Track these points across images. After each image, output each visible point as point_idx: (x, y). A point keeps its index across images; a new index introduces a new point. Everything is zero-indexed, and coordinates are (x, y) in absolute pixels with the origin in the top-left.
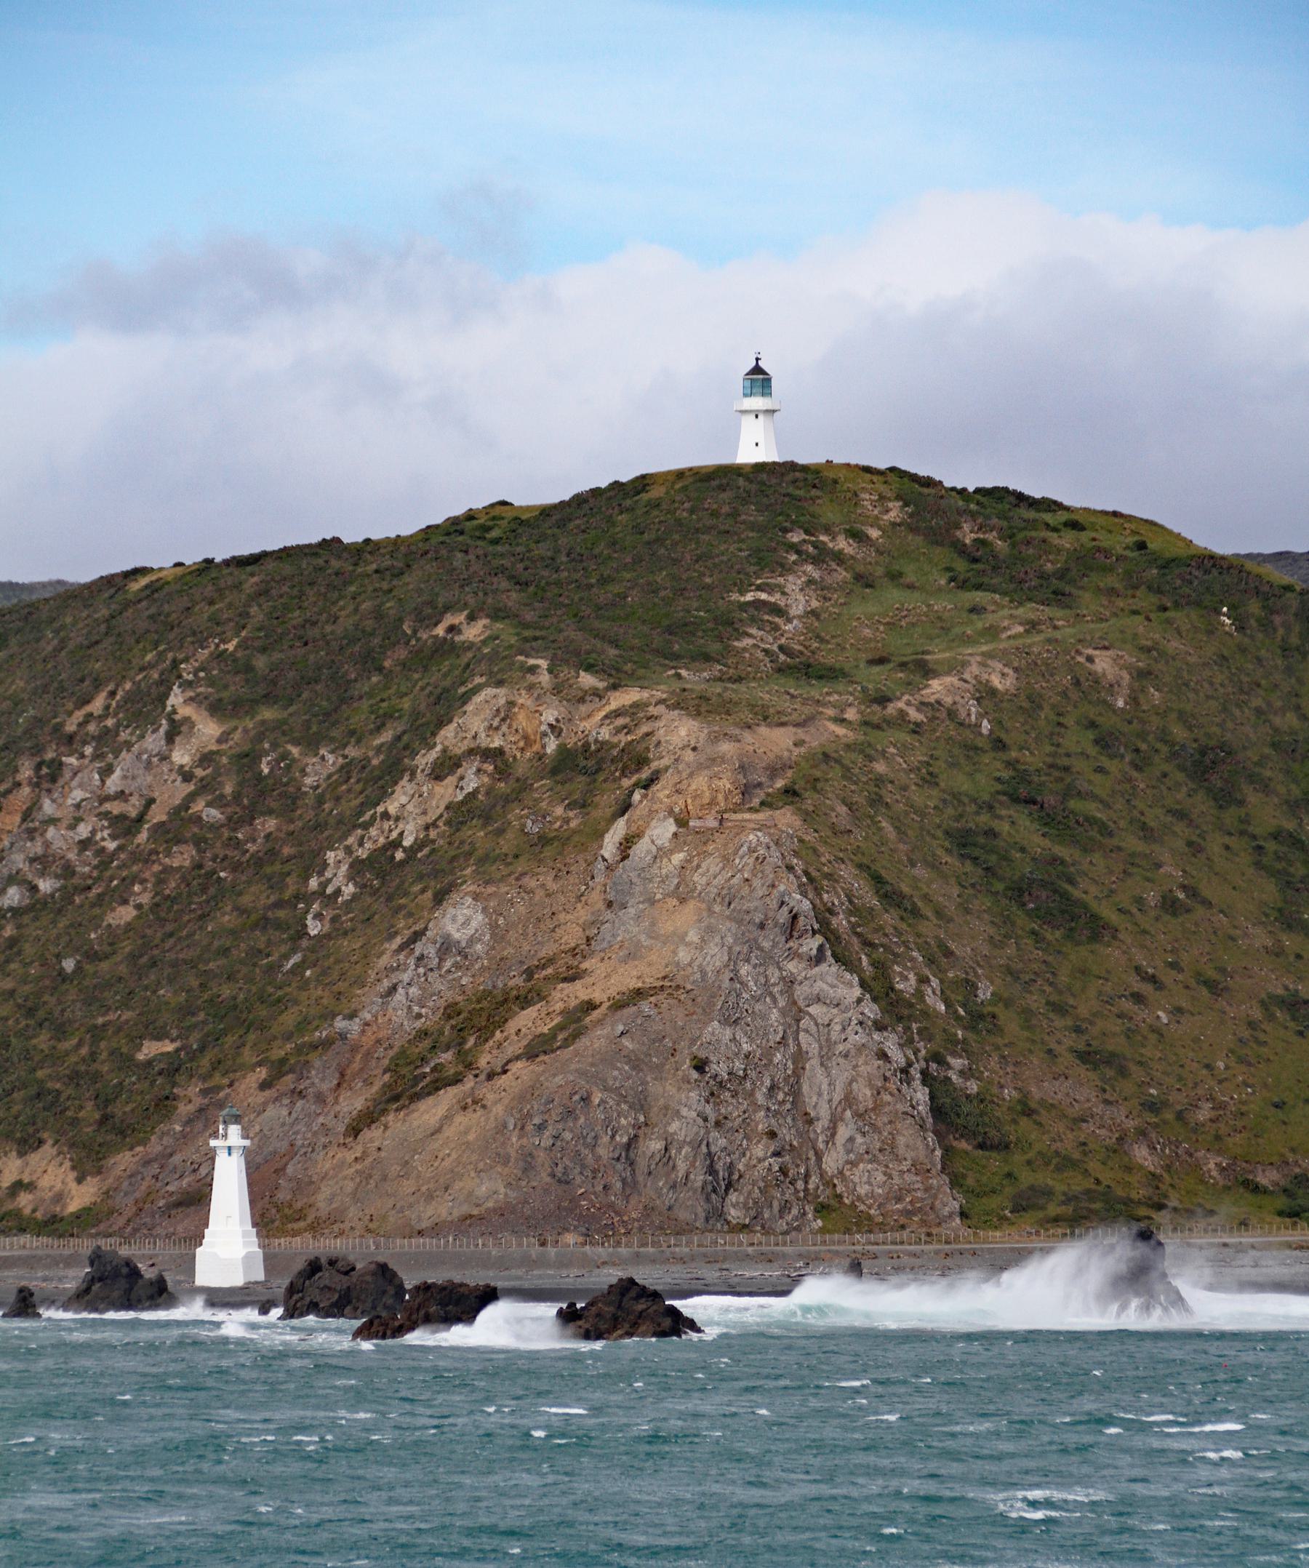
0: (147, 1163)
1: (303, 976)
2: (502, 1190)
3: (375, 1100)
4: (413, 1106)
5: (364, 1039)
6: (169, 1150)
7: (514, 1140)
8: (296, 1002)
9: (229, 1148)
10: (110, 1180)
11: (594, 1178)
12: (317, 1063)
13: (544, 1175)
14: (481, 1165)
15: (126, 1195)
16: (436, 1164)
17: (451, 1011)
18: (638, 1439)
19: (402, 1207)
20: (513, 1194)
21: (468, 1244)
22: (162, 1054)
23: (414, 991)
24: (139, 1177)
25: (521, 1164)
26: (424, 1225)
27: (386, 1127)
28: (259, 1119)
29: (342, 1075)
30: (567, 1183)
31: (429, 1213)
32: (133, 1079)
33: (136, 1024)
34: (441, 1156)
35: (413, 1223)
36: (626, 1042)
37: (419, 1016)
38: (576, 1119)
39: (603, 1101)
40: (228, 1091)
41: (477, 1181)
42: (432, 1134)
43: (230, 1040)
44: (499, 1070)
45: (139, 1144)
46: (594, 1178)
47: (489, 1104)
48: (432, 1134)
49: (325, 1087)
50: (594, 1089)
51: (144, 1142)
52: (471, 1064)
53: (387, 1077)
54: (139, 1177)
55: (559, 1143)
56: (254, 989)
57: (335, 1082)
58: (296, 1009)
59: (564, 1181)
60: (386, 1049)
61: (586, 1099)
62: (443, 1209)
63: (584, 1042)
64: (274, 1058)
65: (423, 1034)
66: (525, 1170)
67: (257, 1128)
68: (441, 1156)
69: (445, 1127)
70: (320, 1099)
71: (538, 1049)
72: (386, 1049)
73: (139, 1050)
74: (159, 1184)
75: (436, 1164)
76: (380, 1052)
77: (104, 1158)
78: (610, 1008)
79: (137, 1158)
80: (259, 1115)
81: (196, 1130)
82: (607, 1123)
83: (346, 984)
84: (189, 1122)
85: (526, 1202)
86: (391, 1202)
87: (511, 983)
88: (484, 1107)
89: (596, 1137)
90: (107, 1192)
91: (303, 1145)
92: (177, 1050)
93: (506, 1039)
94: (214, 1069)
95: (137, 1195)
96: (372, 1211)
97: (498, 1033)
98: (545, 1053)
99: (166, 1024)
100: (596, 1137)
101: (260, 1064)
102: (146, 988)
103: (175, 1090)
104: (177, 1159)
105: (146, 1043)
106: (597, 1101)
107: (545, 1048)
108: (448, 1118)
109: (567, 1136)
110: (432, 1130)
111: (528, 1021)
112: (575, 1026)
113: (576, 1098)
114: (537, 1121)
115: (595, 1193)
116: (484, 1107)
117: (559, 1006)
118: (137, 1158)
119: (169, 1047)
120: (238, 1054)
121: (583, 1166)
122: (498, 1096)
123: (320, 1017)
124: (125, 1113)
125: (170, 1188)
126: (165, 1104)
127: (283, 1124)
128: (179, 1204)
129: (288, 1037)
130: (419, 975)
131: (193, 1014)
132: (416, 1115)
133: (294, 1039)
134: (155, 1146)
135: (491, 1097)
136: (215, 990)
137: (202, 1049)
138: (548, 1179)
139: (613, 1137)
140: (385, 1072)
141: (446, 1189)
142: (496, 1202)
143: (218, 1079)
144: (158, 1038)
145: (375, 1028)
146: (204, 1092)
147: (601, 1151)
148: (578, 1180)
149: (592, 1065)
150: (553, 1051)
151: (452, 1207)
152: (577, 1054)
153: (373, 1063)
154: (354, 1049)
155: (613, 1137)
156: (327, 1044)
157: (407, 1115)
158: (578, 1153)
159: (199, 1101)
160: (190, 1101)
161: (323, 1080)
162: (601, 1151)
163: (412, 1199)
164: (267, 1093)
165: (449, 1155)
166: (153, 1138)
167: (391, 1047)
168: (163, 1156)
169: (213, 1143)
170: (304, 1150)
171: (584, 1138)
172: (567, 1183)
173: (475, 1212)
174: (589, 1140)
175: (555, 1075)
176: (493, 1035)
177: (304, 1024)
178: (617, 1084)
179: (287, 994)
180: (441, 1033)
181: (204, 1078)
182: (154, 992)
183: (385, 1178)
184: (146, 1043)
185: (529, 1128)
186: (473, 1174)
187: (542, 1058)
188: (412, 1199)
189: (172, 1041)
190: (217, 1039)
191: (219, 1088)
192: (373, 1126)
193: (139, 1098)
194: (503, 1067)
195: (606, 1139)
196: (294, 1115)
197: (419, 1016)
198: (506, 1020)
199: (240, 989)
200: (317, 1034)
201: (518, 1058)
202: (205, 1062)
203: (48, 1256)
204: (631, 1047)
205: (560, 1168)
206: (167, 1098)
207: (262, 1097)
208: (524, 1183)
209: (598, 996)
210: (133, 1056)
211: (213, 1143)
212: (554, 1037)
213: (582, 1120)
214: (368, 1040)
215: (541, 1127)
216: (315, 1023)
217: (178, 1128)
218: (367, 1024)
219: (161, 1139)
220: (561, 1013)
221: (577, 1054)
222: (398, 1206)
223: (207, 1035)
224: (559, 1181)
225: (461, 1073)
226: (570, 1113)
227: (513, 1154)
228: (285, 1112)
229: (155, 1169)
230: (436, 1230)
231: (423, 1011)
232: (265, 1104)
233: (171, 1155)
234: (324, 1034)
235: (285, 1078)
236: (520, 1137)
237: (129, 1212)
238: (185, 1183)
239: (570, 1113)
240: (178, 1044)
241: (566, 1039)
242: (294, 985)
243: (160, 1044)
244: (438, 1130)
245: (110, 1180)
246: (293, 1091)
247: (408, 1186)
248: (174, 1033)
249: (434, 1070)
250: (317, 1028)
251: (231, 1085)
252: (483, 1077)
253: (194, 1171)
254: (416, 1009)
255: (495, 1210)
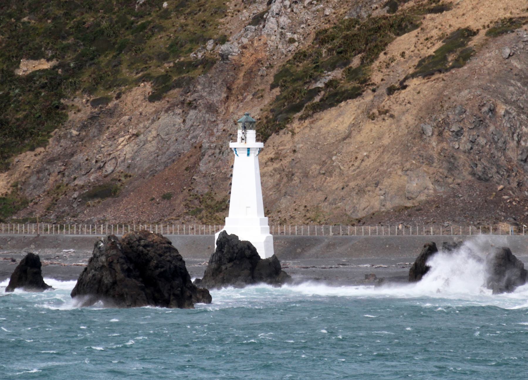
0: (51, 161)
1: (161, 7)
2: (431, 186)
3: (272, 111)
4: (316, 116)
5: (243, 59)
6: (69, 151)
7: (434, 144)
8: (162, 29)
9: (249, 149)
10: (16, 175)
11: (509, 176)
12: (202, 79)
13: (465, 173)
14: (408, 165)
15: (35, 188)
16: (356, 164)
17: (322, 38)
18: (217, 352)
19: (335, 200)
20: (441, 190)
21: (421, 230)
22: (39, 71)
23: (284, 20)
24: (46, 173)
25: (445, 164)
26: (360, 215)
27: (293, 134)
28: (156, 125)
29: (229, 89)
30: (487, 180)
31: (363, 205)
32: (17, 91)
33: (8, 46)
34: (360, 157)
35: (349, 213)
36: (515, 63)
37: (292, 41)
38: (486, 127)
39: (507, 112)
40: (116, 102)
41: (406, 178)
42: (344, 139)
43: (104, 60)
44: (397, 85)
45: (39, 145)
46: (509, 176)
47: (396, 114)
48: (344, 139)
49: (215, 99)
50: (498, 102)
51: (44, 144)
52: (365, 81)
53: (277, 91)
54: (46, 173)
55: (476, 147)
56: (115, 18)
57: (224, 95)
58: (163, 34)
59: (484, 179)
60: (267, 68)
61: (492, 110)
62: (372, 202)
63: (475, 63)
64: (155, 75)
65: (300, 56)
66: (450, 170)
67: (154, 133)
68: (360, 157)
69: (354, 133)
70: (211, 108)
71: (428, 68)
72: (267, 68)
73: (18, 67)
74: (65, 179)
75: (356, 164)
76: (263, 70)
77: (9, 157)
78: (488, 34)
79: (39, 157)
80: (153, 121)
81: (91, 135)
82: (512, 131)
83: (207, 14)
84: (83, 127)
85: (455, 196)
86: (320, 196)
87: (375, 14)
88: (392, 116)
89: (505, 142)
90: (15, 185)
91: (210, 148)
92: (54, 68)
93: (393, 60)
94: (97, 84)
95: (46, 188)
96: (304, 203)
97: (382, 55)
98: (440, 71)
99: (41, 47)
100: (505, 142)
101: (144, 79)
102: (10, 16)
103: (62, 101)
104: (80, 158)
105: (23, 62)
106: (502, 112)
107: (439, 67)
108: (355, 126)
109: (482, 141)
110: (343, 135)
111: (406, 48)
112: (460, 49)
113: (485, 109)
114: (454, 128)
115: (512, 189)
116: (392, 116)
117: (435, 33)
118: (39, 157)
119: (45, 65)
120: (118, 72)
121: (499, 167)
122: (403, 108)
123: (191, 41)
124: (18, 120)
125: (79, 182)
126: (55, 114)
127: (179, 130)
128: (92, 196)
129: (164, 58)
130: (285, 7)
131: (64, 38)
132: (320, 123)
133: (171, 59)
134: (53, 147)
135: (396, 109)
136: (79, 18)
137: (80, 67)
138: (470, 177)
139: (518, 142)
140: (273, 87)
141: (377, 185)
142: (428, 195)
143: (101, 93)
144: (35, 57)
145: (251, 50)
146: (95, 103)
147: (510, 154)
148: (496, 178)
149: (491, 82)
150: (447, 70)
151: (385, 200)
152: (473, 71)
153: (258, 80)
154: (237, 67)
155: (518, 142)
156: (207, 64)
157: (312, 122)
158: (493, 156)
159: (88, 110)
160: (79, 111)
161: (210, 93)
162: (510, 154)
163: (342, 193)
164: (157, 104)
165: (368, 156)
166: (50, 140)
167: (271, 66)
168: (65, 155)
169: (232, 145)
170: (210, 152)
171: (496, 143)
172: (487, 180)
173: (409, 204)
174: (500, 144)
175: (460, 91)
176: (377, 57)
177: (175, 48)
178: (514, 98)
179: (149, 22)
180: (319, 54)
181: (90, 91)
182: (18, 19)
183: (306, 175)
184: (23, 62)
185: (447, 134)
186: (400, 172)
187: (437, 76)
188: (342, 193)
189: (48, 60)
190: (92, 59)
191: (107, 100)
192: (281, 132)
193: (27, 107)
194: (402, 83)
195: (513, 144)
196: (189, 123)
197: (292, 41)
198: (386, 44)
199: (103, 18)
200: (192, 55)
201: (413, 76)
202: (86, 77)
203: (12, 238)
204: (519, 66)
205: (480, 168)
206: (57, 107)
207: (151, 108)
208: (450, 180)
209: (473, 25)
210: (13, 72)
211: (232, 145)
212: (445, 59)
213: (492, 128)
214: (248, 61)
215: (458, 134)
216: (188, 46)
217: (75, 132)
218: (244, 47)
219: (59, 141)
220: (440, 39)
221: (473, 71)
222: (330, 199)
223: (82, 55)
224: (480, 179)
225: (359, 88)
226: (481, 122)
227: (435, 156)
228: (179, 120)
229: (59, 166)
230: (374, 218)
231: (296, 36)
232: (157, 112)
233: (72, 155)
234: (200, 55)
235: (171, 92)
236: (440, 142)
237: (46, 202)
238: (92, 178)
239: (481, 122)
240: (54, 62)
241: (457, 60)
242: (154, 14)
243: (36, 62)
244: (348, 136)
245: (16, 175)
246: (183, 103)
247: (333, 183)
248: (50, 53)
249: (327, 85)
250: (191, 50)
251: (118, 97)
252: (383, 90)
253: (100, 168)
254: (289, 35)
255: (428, 202)
